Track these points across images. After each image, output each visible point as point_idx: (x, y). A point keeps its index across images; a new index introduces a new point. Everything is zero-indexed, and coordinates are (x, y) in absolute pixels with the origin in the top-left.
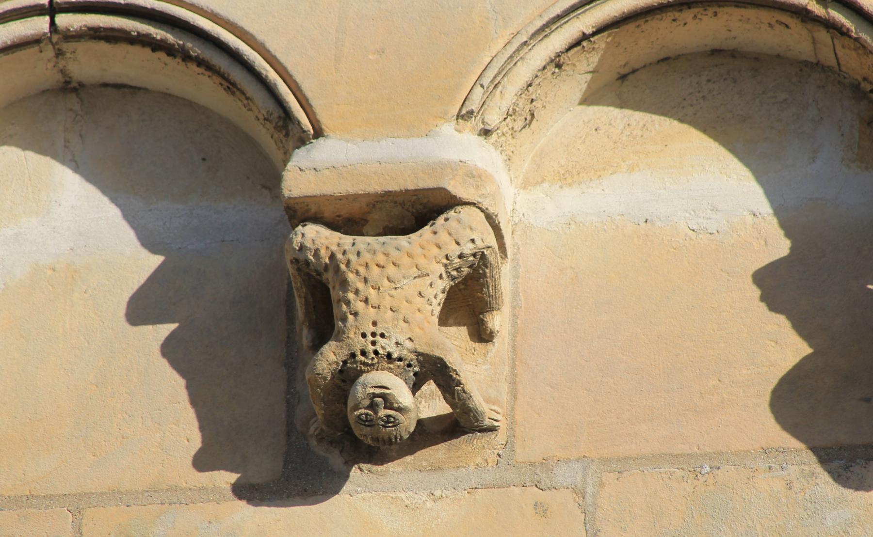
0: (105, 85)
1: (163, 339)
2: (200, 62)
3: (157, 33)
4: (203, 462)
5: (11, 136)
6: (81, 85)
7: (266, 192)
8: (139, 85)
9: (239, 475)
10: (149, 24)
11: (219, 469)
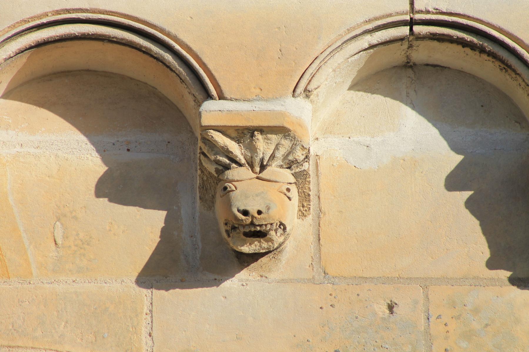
0: (427, 65)
1: (466, 199)
2: (491, 54)
3: (468, 37)
4: (491, 265)
5: (378, 89)
6: (415, 64)
7: (518, 125)
8: (445, 66)
9: (512, 273)
10: (464, 33)
11: (500, 269)
